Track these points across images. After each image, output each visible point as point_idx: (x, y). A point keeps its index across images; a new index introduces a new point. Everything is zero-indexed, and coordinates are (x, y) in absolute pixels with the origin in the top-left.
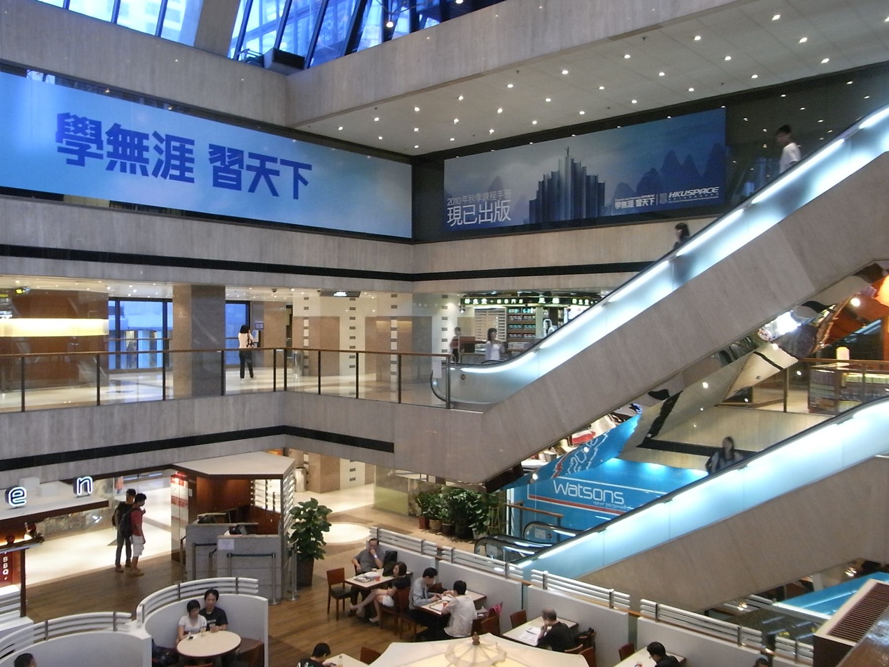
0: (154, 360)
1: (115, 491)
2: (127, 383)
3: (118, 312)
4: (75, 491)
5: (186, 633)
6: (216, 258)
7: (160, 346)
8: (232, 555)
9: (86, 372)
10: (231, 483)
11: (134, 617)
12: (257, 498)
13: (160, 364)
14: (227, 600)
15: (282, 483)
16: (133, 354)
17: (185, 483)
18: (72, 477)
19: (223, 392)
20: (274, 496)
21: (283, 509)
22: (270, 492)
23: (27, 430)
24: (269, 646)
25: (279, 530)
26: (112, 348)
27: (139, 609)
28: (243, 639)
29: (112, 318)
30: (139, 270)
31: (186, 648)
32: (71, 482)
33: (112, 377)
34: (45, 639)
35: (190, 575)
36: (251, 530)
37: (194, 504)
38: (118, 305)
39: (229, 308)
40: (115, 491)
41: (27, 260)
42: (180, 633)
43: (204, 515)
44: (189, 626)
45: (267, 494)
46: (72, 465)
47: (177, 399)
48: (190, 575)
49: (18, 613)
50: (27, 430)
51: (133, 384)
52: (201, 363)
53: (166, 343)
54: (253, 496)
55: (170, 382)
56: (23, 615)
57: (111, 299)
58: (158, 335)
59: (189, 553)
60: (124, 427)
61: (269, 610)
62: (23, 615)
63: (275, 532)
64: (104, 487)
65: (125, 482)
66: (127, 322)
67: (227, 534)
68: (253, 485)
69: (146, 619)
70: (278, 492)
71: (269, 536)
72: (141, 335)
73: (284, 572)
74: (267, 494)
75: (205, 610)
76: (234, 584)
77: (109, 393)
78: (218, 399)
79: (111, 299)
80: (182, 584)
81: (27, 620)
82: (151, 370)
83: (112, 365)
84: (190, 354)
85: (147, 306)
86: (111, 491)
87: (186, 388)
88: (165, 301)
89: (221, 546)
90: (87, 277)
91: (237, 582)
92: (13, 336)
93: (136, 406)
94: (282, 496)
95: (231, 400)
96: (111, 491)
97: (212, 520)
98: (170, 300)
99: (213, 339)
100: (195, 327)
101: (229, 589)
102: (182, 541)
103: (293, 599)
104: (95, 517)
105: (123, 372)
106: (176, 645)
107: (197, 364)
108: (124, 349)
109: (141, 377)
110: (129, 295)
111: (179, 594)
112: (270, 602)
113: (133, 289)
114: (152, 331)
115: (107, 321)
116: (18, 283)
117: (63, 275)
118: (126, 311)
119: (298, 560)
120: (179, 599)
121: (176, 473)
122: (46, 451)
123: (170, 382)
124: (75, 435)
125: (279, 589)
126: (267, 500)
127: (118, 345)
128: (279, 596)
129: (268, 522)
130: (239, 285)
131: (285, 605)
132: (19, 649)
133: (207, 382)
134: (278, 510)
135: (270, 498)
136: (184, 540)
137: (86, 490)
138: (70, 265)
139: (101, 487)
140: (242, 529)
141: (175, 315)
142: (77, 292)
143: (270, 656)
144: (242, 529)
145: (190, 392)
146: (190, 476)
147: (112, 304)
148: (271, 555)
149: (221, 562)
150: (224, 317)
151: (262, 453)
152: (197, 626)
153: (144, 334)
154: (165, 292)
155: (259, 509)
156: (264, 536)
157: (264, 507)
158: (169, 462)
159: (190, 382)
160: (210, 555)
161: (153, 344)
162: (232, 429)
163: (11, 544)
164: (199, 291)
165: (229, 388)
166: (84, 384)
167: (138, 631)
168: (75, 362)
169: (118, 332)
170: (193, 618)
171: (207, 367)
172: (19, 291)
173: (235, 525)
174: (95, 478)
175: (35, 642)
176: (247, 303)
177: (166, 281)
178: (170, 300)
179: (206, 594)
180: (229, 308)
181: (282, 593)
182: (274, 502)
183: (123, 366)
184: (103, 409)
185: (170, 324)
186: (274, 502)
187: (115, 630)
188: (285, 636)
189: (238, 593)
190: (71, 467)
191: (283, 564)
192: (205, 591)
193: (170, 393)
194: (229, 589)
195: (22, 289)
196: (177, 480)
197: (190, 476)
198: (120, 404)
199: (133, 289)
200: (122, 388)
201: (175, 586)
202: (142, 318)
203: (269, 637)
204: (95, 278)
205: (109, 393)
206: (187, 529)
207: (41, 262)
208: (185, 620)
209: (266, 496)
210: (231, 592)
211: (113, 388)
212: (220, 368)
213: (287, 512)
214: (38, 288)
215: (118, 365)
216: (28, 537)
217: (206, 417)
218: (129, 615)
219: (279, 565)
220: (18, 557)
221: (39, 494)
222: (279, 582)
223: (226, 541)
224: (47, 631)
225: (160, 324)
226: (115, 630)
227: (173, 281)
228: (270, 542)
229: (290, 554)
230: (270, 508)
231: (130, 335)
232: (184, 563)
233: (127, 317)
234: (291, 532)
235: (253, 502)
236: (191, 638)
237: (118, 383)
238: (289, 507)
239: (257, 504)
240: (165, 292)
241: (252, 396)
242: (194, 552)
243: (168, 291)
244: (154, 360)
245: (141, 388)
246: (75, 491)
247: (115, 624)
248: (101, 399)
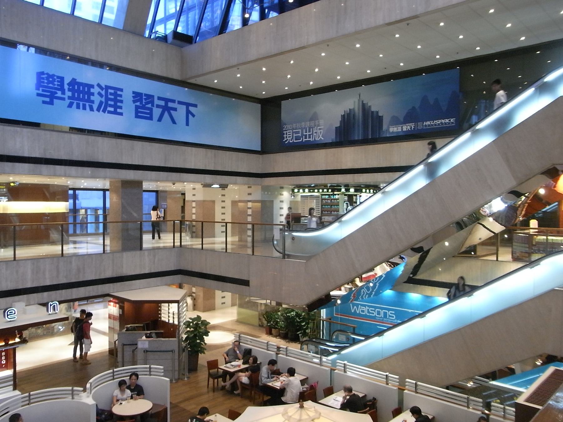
0: (97, 228)
1: (73, 310)
2: (81, 242)
3: (75, 197)
4: (48, 311)
5: (118, 400)
6: (137, 164)
7: (101, 219)
8: (147, 351)
9: (55, 235)
10: (146, 305)
11: (85, 390)
12: (163, 315)
13: (101, 230)
14: (143, 380)
15: (178, 306)
16: (84, 224)
17: (117, 305)
18: (45, 302)
19: (141, 248)
20: (173, 314)
21: (179, 322)
22: (171, 311)
23: (17, 272)
24: (171, 408)
25: (177, 336)
26: (71, 220)
27: (88, 385)
28: (154, 405)
29: (71, 201)
30: (88, 171)
31: (118, 410)
32: (45, 305)
33: (71, 239)
34: (28, 404)
35: (120, 364)
36: (159, 335)
37: (123, 319)
38: (75, 193)
39: (145, 195)
40: (73, 310)
41: (17, 165)
42: (114, 401)
43: (129, 326)
44: (120, 396)
45: (169, 313)
46: (45, 294)
47: (112, 252)
48: (120, 364)
49: (11, 388)
50: (17, 272)
51: (84, 243)
52: (127, 230)
53: (105, 217)
54: (160, 314)
55: (108, 242)
56: (15, 389)
57: (71, 189)
58: (100, 212)
59: (120, 350)
60: (79, 270)
61: (171, 386)
62: (15, 389)
63: (174, 336)
64: (66, 308)
65: (79, 305)
66: (80, 203)
67: (144, 338)
68: (160, 307)
69: (93, 392)
70: (176, 311)
71: (171, 339)
72: (89, 212)
73: (180, 362)
74: (169, 313)
75: (130, 386)
76: (148, 370)
77: (69, 249)
78: (138, 253)
79: (71, 189)
80: (115, 370)
81: (17, 392)
82: (96, 234)
83: (71, 231)
84: (120, 224)
85: (93, 194)
86: (70, 311)
87: (118, 246)
88: (104, 190)
89: (140, 345)
90: (55, 175)
91: (150, 368)
92: (8, 212)
93: (86, 257)
94: (179, 314)
95: (146, 253)
96: (70, 311)
97: (134, 329)
98: (108, 190)
99: (135, 215)
100: (123, 207)
101: (145, 373)
102: (115, 342)
103: (186, 379)
104: (60, 327)
105: (78, 235)
106: (111, 408)
107: (125, 230)
108: (78, 221)
109: (89, 239)
110: (82, 187)
111: (113, 376)
112: (171, 381)
113: (84, 183)
114: (96, 210)
115: (68, 203)
116: (11, 179)
117: (40, 174)
118: (80, 197)
119: (189, 354)
120: (114, 379)
121: (112, 299)
122: (29, 285)
123: (108, 242)
124: (47, 276)
125: (177, 373)
126: (169, 317)
127: (75, 218)
128: (177, 377)
129: (169, 330)
130: (151, 180)
131: (180, 383)
132: (12, 410)
133: (131, 241)
134: (176, 323)
135: (171, 315)
136: (117, 342)
137: (54, 310)
138: (44, 168)
139: (64, 308)
140: (153, 335)
141: (111, 199)
142: (49, 185)
143: (171, 415)
144: (153, 335)
145: (120, 248)
146: (121, 301)
147: (71, 192)
148: (172, 351)
149: (140, 355)
150: (142, 201)
151: (166, 287)
152: (125, 396)
153: (91, 211)
154: (105, 185)
155: (164, 322)
156: (167, 339)
157: (167, 321)
158: (107, 292)
159: (120, 242)
160: (133, 351)
161: (97, 218)
162: (147, 271)
163: (7, 344)
164: (126, 184)
165: (145, 246)
166: (53, 243)
167: (87, 399)
168: (47, 229)
169: (75, 210)
170: (122, 391)
171: (131, 232)
172: (12, 184)
173: (149, 332)
174: (60, 302)
175: (22, 406)
176: (157, 192)
177: (105, 178)
178: (108, 190)
179: (131, 376)
180: (145, 195)
181: (179, 375)
182: (173, 318)
183: (78, 232)
184: (65, 258)
185: (108, 205)
186: (173, 318)
187: (73, 398)
188: (180, 402)
189: (151, 375)
190: (45, 295)
191: (179, 357)
192: (130, 374)
193: (108, 249)
194: (145, 373)
195: (14, 183)
196: (112, 304)
197: (121, 301)
198: (76, 255)
199: (84, 183)
200: (77, 246)
201: (111, 371)
202: (90, 201)
203: (171, 403)
204: (60, 176)
205: (69, 249)
206: (119, 334)
207: (26, 166)
208: (117, 392)
209: (169, 314)
210: (146, 375)
211: (72, 246)
212: (139, 233)
213: (182, 324)
214: (24, 182)
215: (75, 231)
216: (17, 340)
217: (131, 264)
218: (82, 389)
219: (177, 357)
220: (12, 352)
221: (25, 312)
222: (177, 368)
223: (143, 342)
224: (30, 400)
225: (101, 205)
226: (73, 398)
227: (110, 178)
228: (171, 343)
229: (184, 350)
230: (171, 322)
231: (83, 212)
232: (117, 356)
233: (80, 200)
234: (184, 336)
235: (160, 318)
236: (121, 404)
237: (75, 242)
238: (183, 321)
239: (163, 319)
240: (105, 185)
241: (160, 250)
242: (123, 349)
243: (106, 184)
244: (97, 228)
245: (89, 246)
246: (48, 311)
247: (73, 395)
248: (64, 252)
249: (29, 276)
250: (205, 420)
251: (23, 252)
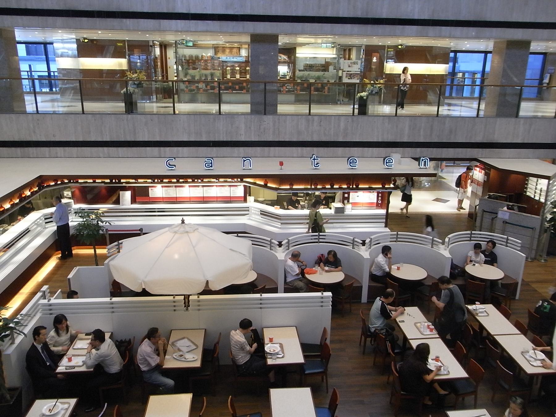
0: (473, 92)
1: (440, 170)
2: (455, 105)
3: (455, 60)
4: (419, 165)
5: (471, 261)
6: (528, 21)
7: (478, 82)
8: (506, 223)
9: (431, 97)
10: (513, 176)
11: (443, 243)
12: (528, 190)
13: (477, 94)
14: (500, 249)
15: (549, 182)
16: (461, 87)
17: (483, 171)
18: (418, 157)
19: (517, 116)
20: (541, 191)
21: (546, 200)
22: (539, 187)
23: (397, 126)
24: (522, 285)
25: (541, 214)
26: (449, 82)
27: (447, 240)
28: (505, 275)
29: (451, 64)
30: (472, 31)
31: (470, 269)
32: (417, 159)
33: (447, 101)
34: (395, 241)
35: (478, 228)
36: (521, 210)
37: (487, 186)
38: (455, 55)
39: (531, 58)
40: (440, 170)
41: (407, 27)
42: (468, 261)
43: (492, 194)
44: (473, 258)
45: (536, 188)
46: (419, 150)
47: (485, 117)
48: (478, 228)
49: (383, 225)
50: (397, 126)
51: (458, 106)
52: (505, 95)
53: (483, 81)
54: (526, 188)
55: (483, 106)
56: (386, 226)
57: (452, 51)
58: (478, 76)
59: (479, 215)
60: (451, 132)
61: (525, 263)
62: (386, 226)
63: (538, 214)
64: (434, 167)
65: (446, 166)
66: (459, 66)
67: (505, 208)
68: (527, 180)
69: (450, 247)
70: (545, 188)
71: (533, 216)
72: (467, 75)
73: (539, 241)
74: (536, 188)
75: (485, 251)
76: (506, 241)
77: (444, 110)
78: (513, 120)
79: (452, 51)
80: (473, 232)
81: (387, 230)
82: (471, 98)
83: (447, 94)
84: (498, 88)
85: (474, 54)
86: (438, 170)
87: (493, 111)
88: (486, 53)
89: (500, 215)
90: (441, 36)
91: (507, 239)
92: (394, 73)
93: (460, 119)
94: (548, 191)
95: (522, 121)
96: (438, 170)
97: (496, 198)
98: (490, 52)
99: (515, 79)
100: (504, 70)
101: (502, 243)
102: (476, 207)
103: (543, 261)
104: (426, 184)
105: (453, 98)
106: (465, 266)
107: (503, 95)
108: (455, 83)
109: (464, 102)
110: (464, 49)
111: (471, 237)
112: (527, 258)
113: (467, 45)
114: (474, 73)
115: (447, 65)
116: (400, 41)
117: (426, 36)
118: (459, 60)
119: (551, 237)
120: (471, 240)
121: (478, 164)
122: (405, 140)
123: (483, 106)
124: (422, 132)
125: (534, 252)
126: (535, 192)
127: (452, 81)
128: (533, 256)
129: (535, 207)
130: (542, 40)
131: (535, 263)
132: (383, 243)
133: (508, 107)
134: (543, 200)
135: (538, 191)
136: (477, 207)
137: (425, 165)
138: (431, 30)
139: (432, 166)
140: (515, 208)
141: (492, 62)
142: (432, 47)
143: (521, 291)
144: (515, 208)
145: (495, 114)
146: (487, 167)
147: (452, 55)
148: (532, 229)
149: (498, 225)
150: (527, 63)
151: (538, 160)
152: (478, 259)
153: (469, 75)
154: (487, 46)
155: (529, 197)
156: (529, 215)
157: (533, 197)
158: (476, 157)
159: (496, 107)
160: (493, 219)
161: (474, 82)
162: (519, 141)
163: (383, 187)
164: (512, 44)
165: (522, 113)
166: (430, 104)
167: (445, 252)
168: (426, 91)
169: (453, 73)
170: (476, 254)
171: (509, 98)
172: (400, 47)
173: (511, 204)
174: (431, 159)
175: (391, 242)
176: (545, 54)
177: (489, 38)
178: (490, 52)
179: (488, 242)
180: (531, 58)
181: (536, 256)
182: (540, 195)
183: (454, 95)
184: (440, 119)
185: (488, 69)
186: (540, 195)
187: (432, 247)
188: (532, 282)
189: (507, 246)
190: (418, 151)
191: (540, 236)
192: (488, 240)
193: (482, 113)
194: (502, 243)
195: (401, 45)
196: (478, 169)
197: (487, 167)
198: (448, 116)
199: (467, 45)
200: (451, 108)
201: (469, 232)
202: (470, 64)
203: (523, 280)
204: (445, 37)
205: (444, 110)
206: (480, 200)
207: (414, 28)
208: (471, 253)
209: (536, 189)
210: (502, 245)
211: (446, 107)
212: (518, 100)
213: (549, 203)
214: (410, 44)
215: (451, 94)
216: (392, 186)
217: (503, 130)
218: (440, 241)
219: (537, 236)
220: (387, 195)
221: (400, 163)
222: (535, 247)
223: (504, 213)
224: (397, 238)
225: (481, 69)
226: (432, 247)
227: (495, 38)
228: (533, 220)
229: (546, 231)
230: (537, 198)
231: (460, 75)
232: (475, 221)
233: (459, 64)
234: (549, 216)
235: (526, 192)
236: (474, 265)
237: (449, 105)
238: (552, 199)
239: (528, 194)
240: (487, 46)
241: (538, 120)
242: (483, 215)
243: (489, 45)
244: (473, 92)
245: (463, 109)
246: (419, 165)
247: (432, 244)
248: (439, 113)
249: (242, 132)
250: (73, 401)
251: (317, 109)
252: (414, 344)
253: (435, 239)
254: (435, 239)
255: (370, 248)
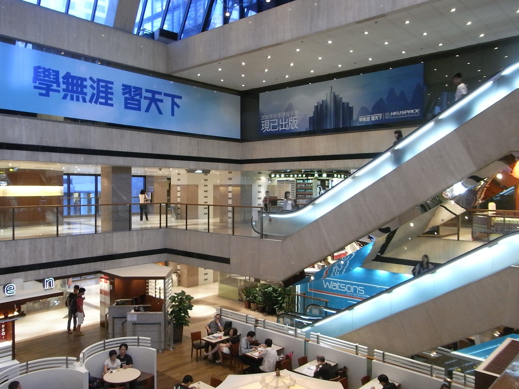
0: (90, 210)
1: (67, 286)
2: (74, 223)
3: (69, 182)
4: (44, 286)
5: (108, 369)
6: (126, 151)
7: (93, 202)
8: (136, 324)
9: (50, 217)
10: (135, 281)
11: (78, 360)
12: (150, 290)
13: (93, 212)
14: (132, 350)
15: (164, 282)
16: (78, 207)
17: (108, 281)
18: (42, 278)
19: (130, 229)
20: (160, 289)
21: (165, 297)
22: (158, 287)
23: (16, 251)
24: (157, 377)
25: (163, 309)
26: (65, 203)
27: (81, 355)
28: (142, 373)
29: (66, 185)
30: (81, 157)
31: (109, 378)
32: (42, 281)
33: (66, 220)
34: (26, 373)
35: (111, 335)
36: (146, 309)
37: (113, 294)
38: (69, 178)
39: (134, 180)
40: (67, 286)
41: (16, 152)
42: (105, 369)
43: (119, 300)
44: (110, 365)
45: (156, 288)
46: (42, 271)
47: (104, 232)
48: (111, 335)
49: (10, 357)
50: (16, 251)
51: (78, 224)
52: (117, 212)
53: (97, 200)
54: (148, 290)
55: (99, 223)
56: (13, 358)
57: (65, 174)
58: (92, 195)
59: (110, 322)
60: (72, 249)
61: (157, 356)
62: (13, 358)
63: (160, 310)
64: (61, 284)
65: (73, 281)
66: (74, 188)
67: (133, 311)
68: (148, 283)
69: (85, 361)
70: (162, 287)
71: (157, 312)
72: (82, 195)
73: (166, 333)
74: (156, 288)
75: (119, 355)
76: (137, 341)
77: (64, 229)
78: (127, 233)
79: (65, 174)
80: (106, 341)
81: (16, 362)
82: (88, 216)
83: (65, 213)
84: (111, 206)
85: (86, 178)
86: (65, 287)
87: (109, 226)
88: (96, 176)
89: (129, 318)
90: (51, 161)
91: (138, 339)
92: (8, 196)
93: (79, 237)
94: (165, 289)
95: (135, 233)
96: (65, 287)
97: (124, 303)
98: (99, 175)
99: (125, 198)
100: (114, 191)
101: (134, 344)
102: (106, 315)
103: (171, 349)
104: (55, 302)
105: (72, 217)
106: (103, 376)
107: (115, 212)
108: (72, 203)
109: (82, 220)
110: (76, 172)
111: (104, 347)
112: (158, 351)
113: (78, 169)
114: (88, 193)
115: (62, 187)
116: (10, 165)
117: (37, 160)
118: (73, 182)
119: (174, 327)
120: (105, 349)
121: (103, 276)
122: (27, 263)
123: (99, 223)
124: (44, 254)
125: (163, 344)
126: (156, 292)
127: (69, 201)
128: (163, 347)
129: (156, 305)
130: (139, 166)
131: (166, 353)
132: (11, 378)
133: (121, 223)
134: (162, 297)
135: (158, 291)
136: (108, 315)
137: (50, 285)
138: (41, 155)
139: (59, 284)
140: (141, 309)
141: (102, 184)
142: (45, 170)
143: (157, 382)
144: (141, 309)
145: (111, 229)
146: (111, 278)
147: (65, 177)
148: (158, 324)
149: (129, 328)
150: (131, 185)
151: (153, 264)
152: (115, 365)
153: (84, 195)
154: (96, 170)
155: (151, 297)
156: (154, 313)
157: (154, 296)
158: (99, 270)
159: (111, 223)
160: (123, 324)
161: (89, 201)
162: (135, 250)
163: (6, 317)
164: (116, 170)
165: (133, 226)
166: (49, 224)
167: (80, 368)
168: (44, 211)
169: (69, 194)
170: (113, 361)
171: (121, 214)
172: (11, 170)
173: (137, 306)
174: (56, 279)
175: (21, 374)
176: (144, 177)
177: (97, 164)
178: (99, 175)
179: (121, 347)
180: (134, 180)
181: (165, 346)
182: (160, 293)
183: (72, 214)
184: (60, 238)
185: (99, 189)
186: (160, 293)
187: (67, 367)
188: (166, 371)
189: (139, 346)
190: (42, 272)
191: (165, 329)
192: (120, 345)
193: (99, 229)
194: (134, 344)
195: (13, 168)
196: (103, 280)
197: (111, 278)
198: (70, 235)
199: (78, 169)
200: (71, 226)
201: (102, 342)
202: (83, 185)
203: (157, 371)
204: (55, 162)
205: (64, 229)
206: (109, 308)
207: (24, 153)
208: (108, 362)
209: (156, 289)
210: (135, 345)
211: (66, 226)
212: (128, 214)
213: (168, 299)
214: (22, 168)
215: (69, 213)
216: (16, 313)
217: (120, 243)
218: (75, 358)
219: (163, 329)
220: (11, 325)
221: (23, 288)
222: (163, 339)
223: (132, 315)
224: (27, 368)
225: (93, 189)
226: (67, 367)
227: (101, 164)
228: (157, 316)
229: (169, 323)
230: (158, 296)
231: (76, 195)
232: (108, 328)
233: (74, 185)
234: (170, 310)
235: (148, 293)
236: (112, 372)
237: (69, 223)
238: (169, 296)
239: (150, 294)
240: (96, 170)
241: (147, 231)
242: (113, 322)
243: (98, 170)
244: (90, 210)
245: (82, 227)
246: (44, 286)
247: (67, 364)
248: (59, 233)
252: (397, 384)
253: (140, 338)
254: (140, 338)
255: (84, 362)
